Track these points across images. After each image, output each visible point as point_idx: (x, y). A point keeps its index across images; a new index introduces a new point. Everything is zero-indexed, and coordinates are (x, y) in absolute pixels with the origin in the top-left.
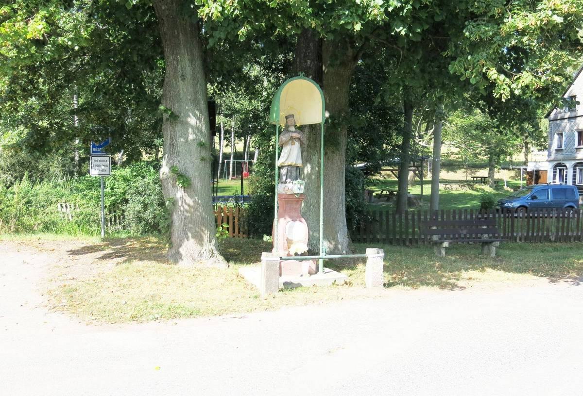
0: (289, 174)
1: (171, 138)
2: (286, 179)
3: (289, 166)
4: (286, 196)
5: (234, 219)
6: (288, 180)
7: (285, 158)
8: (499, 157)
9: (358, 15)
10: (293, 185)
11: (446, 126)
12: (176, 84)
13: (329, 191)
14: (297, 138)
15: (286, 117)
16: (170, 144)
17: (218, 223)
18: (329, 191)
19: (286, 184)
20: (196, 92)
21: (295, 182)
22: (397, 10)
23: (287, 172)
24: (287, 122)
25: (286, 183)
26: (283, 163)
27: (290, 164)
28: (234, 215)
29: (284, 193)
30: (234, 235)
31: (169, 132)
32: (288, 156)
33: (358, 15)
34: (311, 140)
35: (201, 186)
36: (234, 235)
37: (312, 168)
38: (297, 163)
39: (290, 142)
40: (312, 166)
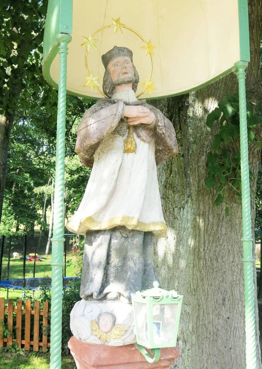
0: (115, 260)
2: (105, 283)
3: (114, 229)
4: (104, 355)
5: (41, 319)
6: (114, 288)
7: (103, 199)
9: (188, 104)
10: (130, 308)
13: (224, 300)
17: (17, 326)
18: (224, 300)
19: (108, 306)
21: (137, 296)
23: (108, 256)
24: (107, 73)
25: (105, 298)
26: (90, 219)
27: (118, 222)
28: (42, 314)
29: (93, 340)
30: (41, 344)
32: (112, 194)
33: (188, 104)
34: (175, 169)
36: (41, 344)
37: (179, 241)
38: (146, 220)
39: (119, 141)
40: (178, 234)
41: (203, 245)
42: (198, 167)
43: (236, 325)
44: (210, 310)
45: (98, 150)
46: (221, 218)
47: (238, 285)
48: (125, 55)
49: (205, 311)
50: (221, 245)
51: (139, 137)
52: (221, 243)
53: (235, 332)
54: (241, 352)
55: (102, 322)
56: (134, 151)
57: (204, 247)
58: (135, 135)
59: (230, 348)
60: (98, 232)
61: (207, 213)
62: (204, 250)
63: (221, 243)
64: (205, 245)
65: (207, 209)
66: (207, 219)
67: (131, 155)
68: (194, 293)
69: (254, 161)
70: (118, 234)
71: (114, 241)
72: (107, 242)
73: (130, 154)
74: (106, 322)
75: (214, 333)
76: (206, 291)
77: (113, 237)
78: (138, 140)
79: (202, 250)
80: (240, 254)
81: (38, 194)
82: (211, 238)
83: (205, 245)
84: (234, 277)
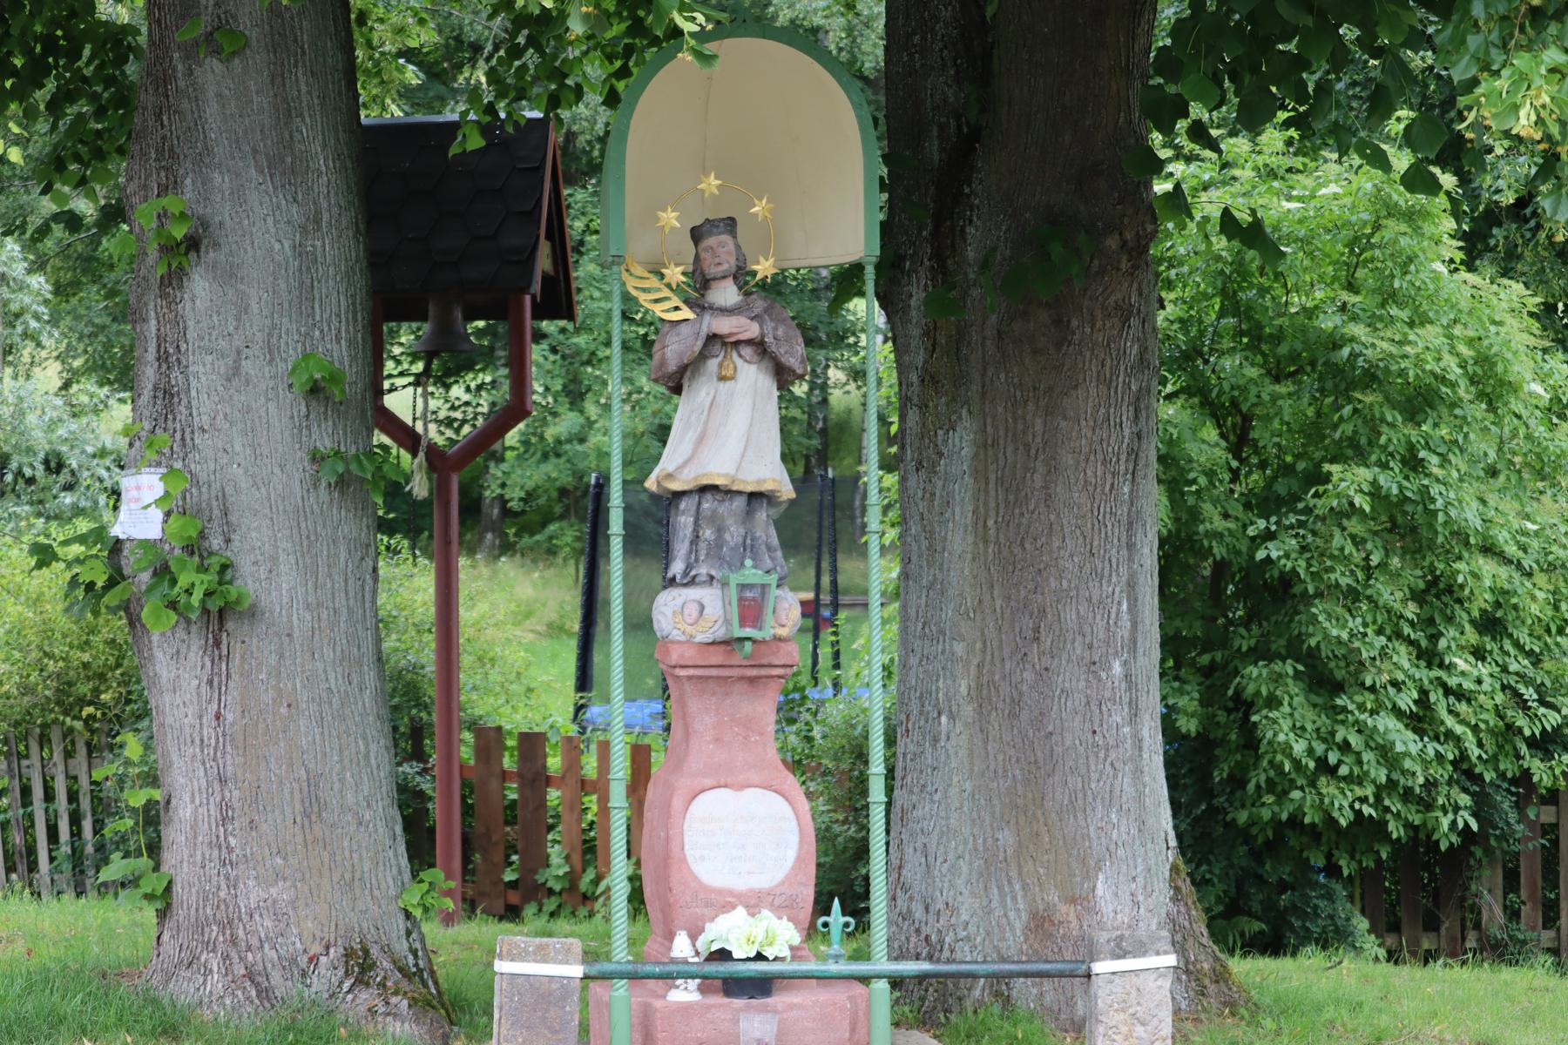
1: (163, 358)
8: (1522, 203)
11: (1428, 475)
12: (190, 72)
13: (1037, 630)
14: (749, 342)
15: (693, 230)
16: (156, 389)
20: (286, 113)
22: (1220, 19)
24: (697, 258)
31: (153, 323)
35: (308, 606)
41: (992, 513)
42: (984, 338)
43: (1067, 685)
44: (1006, 651)
45: (688, 374)
46: (1033, 452)
47: (1074, 600)
48: (720, 234)
49: (996, 654)
50: (1033, 512)
51: (740, 356)
52: (1031, 507)
53: (1063, 700)
54: (1077, 742)
55: (686, 612)
56: (732, 378)
57: (997, 516)
58: (735, 355)
59: (1051, 734)
60: (683, 493)
61: (1001, 441)
62: (996, 522)
63: (1031, 507)
64: (998, 513)
65: (1002, 433)
66: (1001, 455)
67: (729, 384)
68: (972, 615)
69: (1108, 324)
70: (709, 496)
71: (705, 506)
72: (694, 508)
73: (728, 383)
74: (693, 610)
75: (1013, 700)
76: (999, 610)
77: (704, 501)
78: (739, 362)
79: (990, 523)
80: (1078, 532)
81: (759, 277)
82: (1011, 497)
83: (998, 513)
84: (1065, 583)
